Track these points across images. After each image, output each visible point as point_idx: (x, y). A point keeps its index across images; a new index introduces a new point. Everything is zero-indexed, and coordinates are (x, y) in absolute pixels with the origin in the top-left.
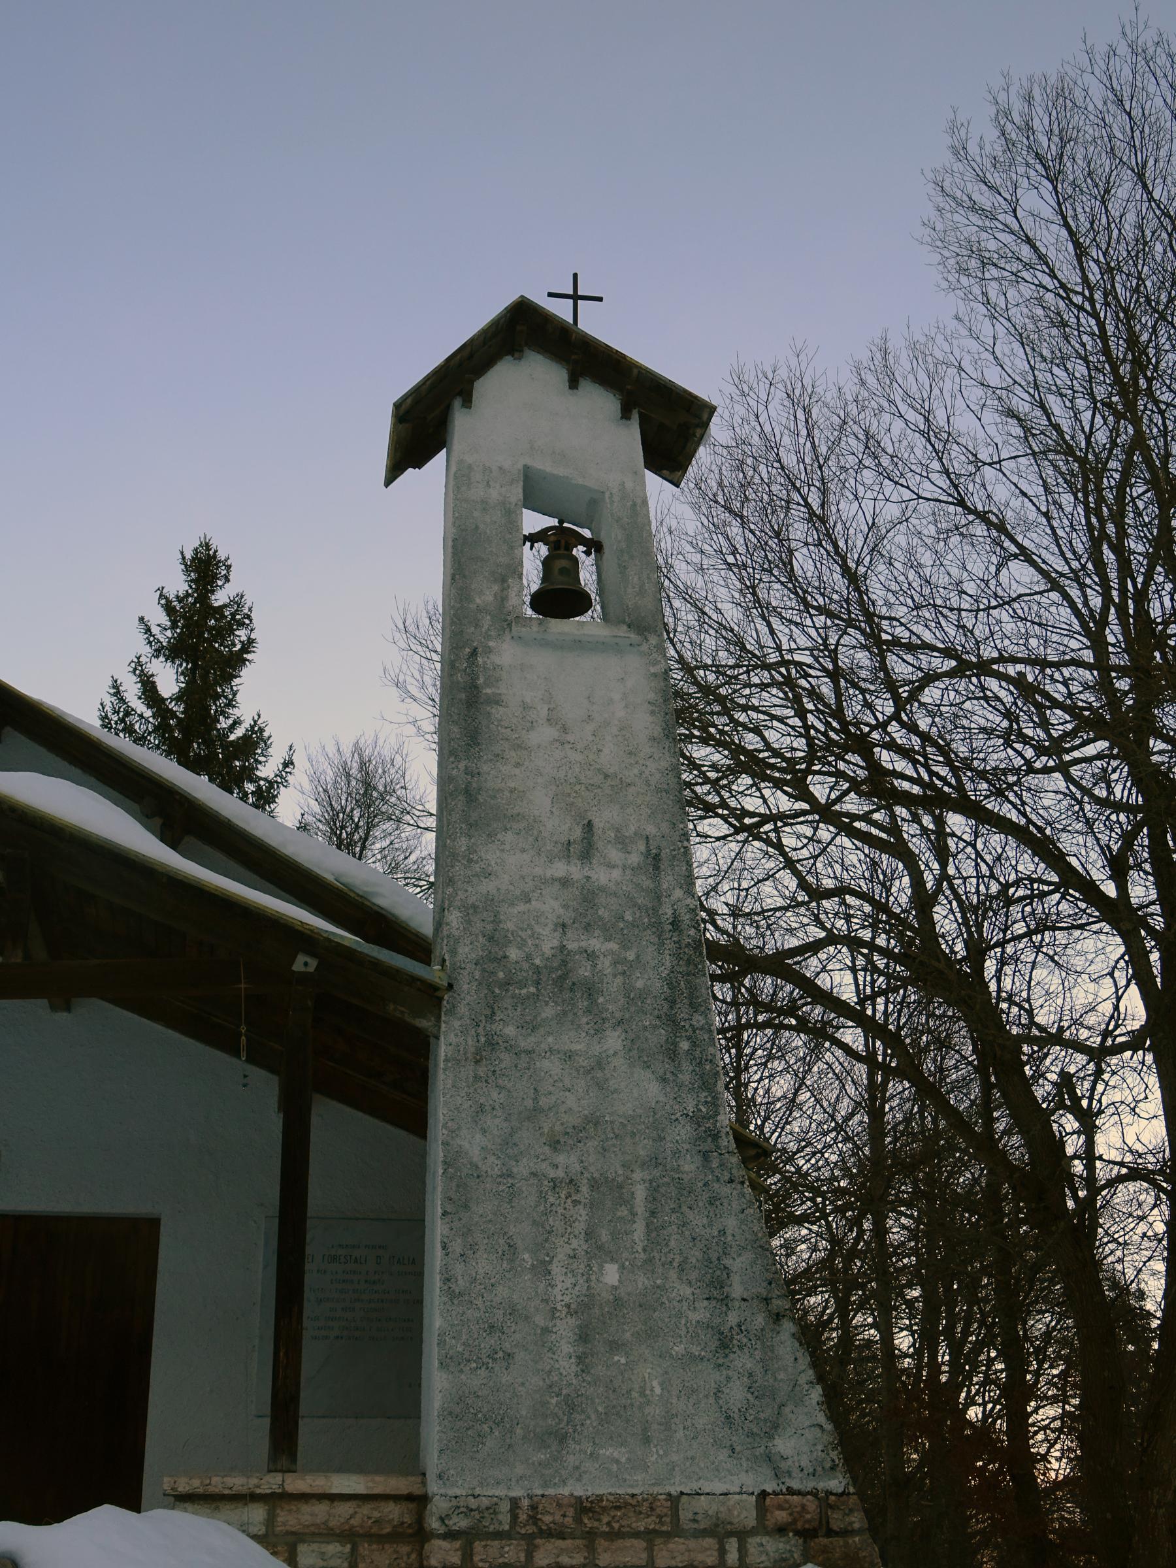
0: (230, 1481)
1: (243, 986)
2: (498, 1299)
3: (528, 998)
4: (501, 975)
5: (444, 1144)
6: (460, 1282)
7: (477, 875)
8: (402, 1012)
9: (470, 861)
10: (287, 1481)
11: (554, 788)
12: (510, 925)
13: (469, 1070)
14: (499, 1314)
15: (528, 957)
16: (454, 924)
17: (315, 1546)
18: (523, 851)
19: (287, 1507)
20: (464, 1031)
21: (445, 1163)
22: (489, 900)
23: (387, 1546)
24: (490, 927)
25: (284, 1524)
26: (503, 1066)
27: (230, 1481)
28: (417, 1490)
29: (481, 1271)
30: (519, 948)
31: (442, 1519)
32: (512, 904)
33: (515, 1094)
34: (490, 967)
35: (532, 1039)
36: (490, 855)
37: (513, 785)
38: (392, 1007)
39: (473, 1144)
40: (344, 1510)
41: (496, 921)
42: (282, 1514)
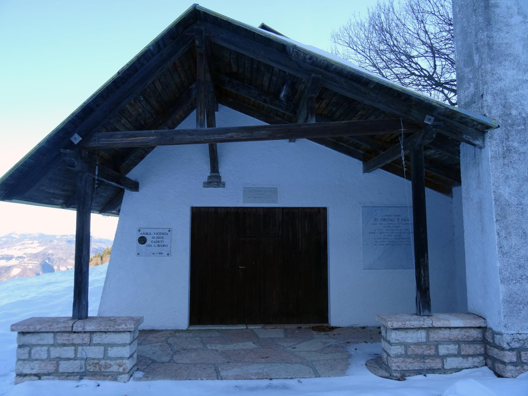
0: (413, 323)
1: (402, 130)
2: (521, 255)
3: (522, 130)
4: (510, 121)
5: (494, 192)
6: (506, 248)
7: (495, 80)
8: (469, 138)
9: (493, 74)
10: (434, 322)
11: (523, 42)
12: (511, 100)
13: (501, 161)
14: (522, 261)
15: (520, 114)
16: (489, 101)
17: (445, 346)
18: (513, 69)
19: (433, 331)
20: (498, 145)
21: (495, 200)
22: (502, 90)
23: (471, 345)
24: (503, 101)
25: (433, 338)
26: (514, 159)
27: (413, 323)
28: (483, 325)
29: (513, 244)
30: (516, 110)
31: (508, 344)
32: (511, 92)
33: (520, 171)
34: (505, 118)
35: (525, 148)
36: (500, 71)
37: (506, 41)
38: (465, 136)
39: (505, 192)
40: (455, 332)
41: (506, 98)
42: (431, 334)
